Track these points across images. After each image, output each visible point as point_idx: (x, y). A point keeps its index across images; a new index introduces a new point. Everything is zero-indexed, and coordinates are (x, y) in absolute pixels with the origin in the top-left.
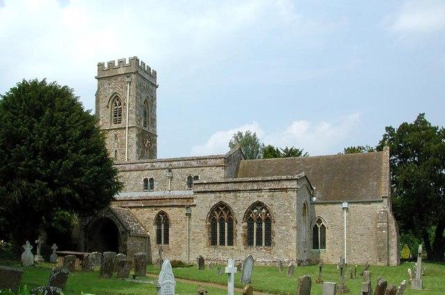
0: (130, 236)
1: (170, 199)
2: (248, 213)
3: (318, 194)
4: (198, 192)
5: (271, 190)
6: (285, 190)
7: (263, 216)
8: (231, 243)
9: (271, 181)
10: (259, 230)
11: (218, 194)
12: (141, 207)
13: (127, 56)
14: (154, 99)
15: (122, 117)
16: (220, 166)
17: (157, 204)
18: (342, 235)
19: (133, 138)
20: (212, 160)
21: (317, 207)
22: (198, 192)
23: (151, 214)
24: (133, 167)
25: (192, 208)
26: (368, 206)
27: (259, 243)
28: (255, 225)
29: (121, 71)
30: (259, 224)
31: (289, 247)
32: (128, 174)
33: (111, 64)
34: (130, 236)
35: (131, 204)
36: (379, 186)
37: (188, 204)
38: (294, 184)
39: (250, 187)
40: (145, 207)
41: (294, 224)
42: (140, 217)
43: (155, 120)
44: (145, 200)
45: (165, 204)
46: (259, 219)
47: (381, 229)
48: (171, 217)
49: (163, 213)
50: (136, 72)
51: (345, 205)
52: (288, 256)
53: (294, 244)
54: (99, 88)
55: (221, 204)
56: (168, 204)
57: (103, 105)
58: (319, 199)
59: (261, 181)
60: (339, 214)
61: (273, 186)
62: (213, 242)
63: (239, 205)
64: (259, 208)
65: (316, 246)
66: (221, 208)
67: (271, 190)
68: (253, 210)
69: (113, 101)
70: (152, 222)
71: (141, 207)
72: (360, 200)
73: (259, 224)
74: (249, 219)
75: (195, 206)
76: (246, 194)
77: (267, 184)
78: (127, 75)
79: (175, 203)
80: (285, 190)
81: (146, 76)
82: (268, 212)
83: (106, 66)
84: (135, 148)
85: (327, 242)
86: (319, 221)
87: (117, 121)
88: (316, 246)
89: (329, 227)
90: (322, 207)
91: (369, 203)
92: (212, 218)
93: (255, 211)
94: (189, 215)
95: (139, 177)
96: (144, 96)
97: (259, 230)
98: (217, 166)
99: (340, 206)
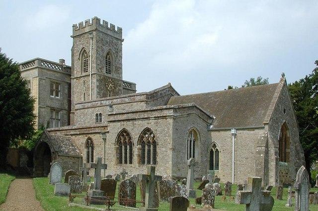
0: (59, 156)
1: (94, 128)
2: (141, 137)
3: (216, 123)
4: (111, 121)
5: (157, 118)
6: (164, 117)
7: (152, 139)
8: (131, 162)
9: (157, 110)
10: (149, 151)
11: (122, 123)
12: (77, 134)
13: (90, 17)
14: (119, 51)
15: (88, 63)
16: (143, 101)
17: (86, 132)
18: (231, 159)
19: (94, 83)
20: (138, 97)
21: (213, 133)
22: (111, 121)
23: (82, 140)
24: (89, 105)
25: (107, 134)
26: (252, 132)
27: (126, 162)
28: (146, 147)
29: (87, 30)
30: (149, 146)
31: (167, 165)
32: (86, 110)
33: (81, 24)
34: (59, 156)
35: (72, 133)
36: (264, 115)
37: (103, 131)
38: (171, 113)
39: (142, 116)
40: (80, 134)
41: (170, 146)
42: (77, 142)
43: (121, 68)
44: (79, 129)
45: (91, 132)
46: (149, 142)
47: (259, 153)
48: (95, 142)
49: (89, 139)
50: (96, 30)
51: (233, 131)
52: (166, 173)
53: (171, 163)
54: (74, 45)
55: (147, 131)
56: (93, 131)
57: (76, 58)
58: (215, 126)
59: (149, 111)
60: (229, 139)
61: (157, 114)
62: (121, 162)
63: (135, 130)
64: (149, 133)
65: (211, 168)
66: (124, 133)
67: (157, 118)
68: (145, 135)
69: (82, 55)
70: (84, 146)
71: (77, 134)
72: (246, 127)
73: (149, 146)
74: (141, 139)
75: (108, 132)
76: (140, 122)
77: (153, 113)
78: (90, 32)
79: (97, 130)
80: (164, 117)
81: (109, 32)
82: (154, 136)
83: (78, 26)
84: (96, 90)
85: (220, 164)
86: (215, 146)
87: (86, 70)
88: (211, 168)
89: (222, 150)
90: (217, 133)
91: (253, 129)
92: (118, 141)
93: (147, 136)
94: (105, 140)
95: (93, 113)
96: (106, 49)
97: (149, 151)
98: (141, 102)
99: (228, 133)
